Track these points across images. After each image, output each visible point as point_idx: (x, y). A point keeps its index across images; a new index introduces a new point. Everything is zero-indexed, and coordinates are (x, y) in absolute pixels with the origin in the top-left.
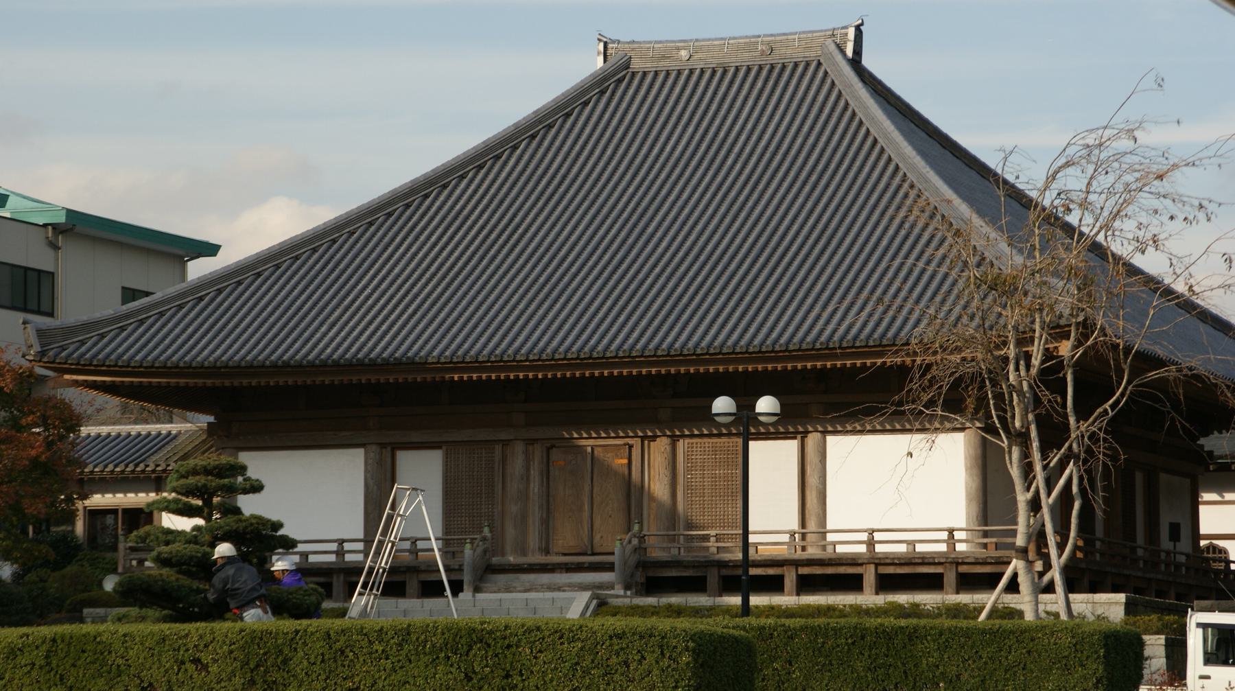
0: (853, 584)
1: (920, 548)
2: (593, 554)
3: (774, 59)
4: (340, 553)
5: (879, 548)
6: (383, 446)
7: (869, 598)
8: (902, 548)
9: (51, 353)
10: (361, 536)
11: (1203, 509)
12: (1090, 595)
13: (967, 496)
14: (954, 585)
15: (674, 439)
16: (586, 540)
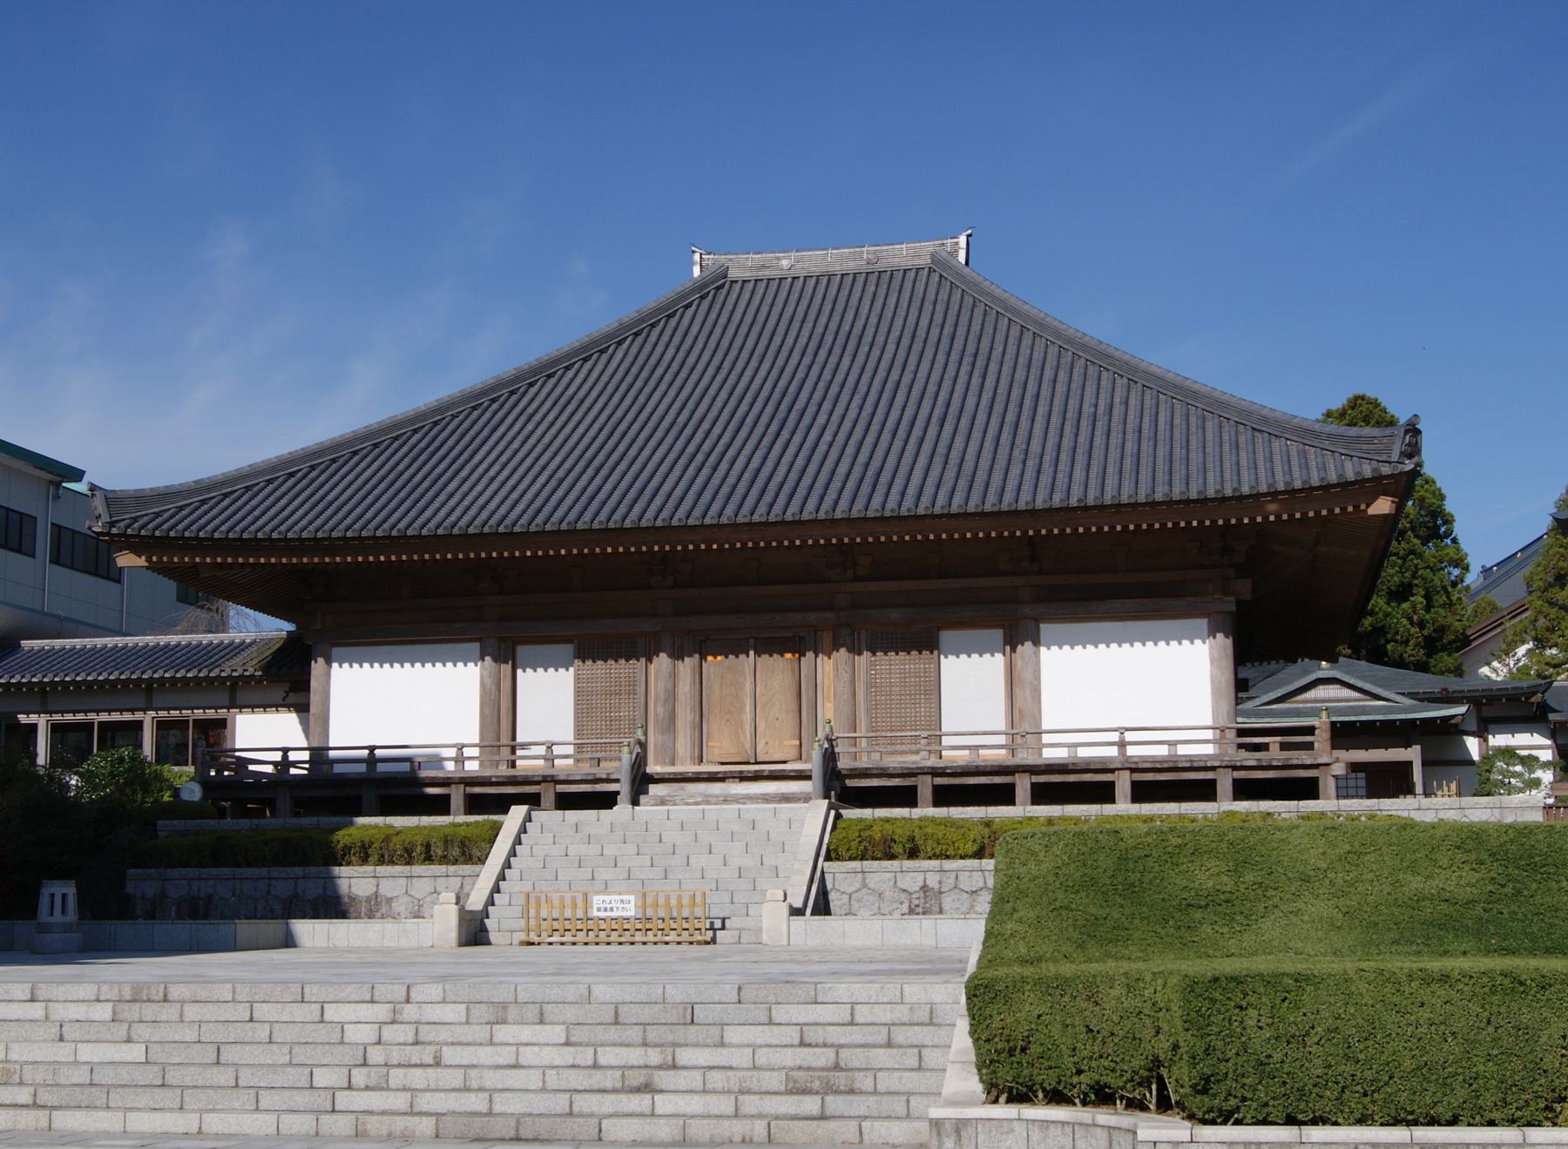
0: (1104, 793)
1: (1182, 750)
2: (757, 763)
3: (879, 267)
4: (550, 758)
5: (1132, 751)
6: (501, 639)
7: (1022, 809)
8: (1162, 751)
9: (122, 525)
10: (477, 741)
11: (1000, 723)
12: (1295, 803)
13: (1213, 693)
14: (1230, 794)
15: (703, 658)
16: (748, 746)
